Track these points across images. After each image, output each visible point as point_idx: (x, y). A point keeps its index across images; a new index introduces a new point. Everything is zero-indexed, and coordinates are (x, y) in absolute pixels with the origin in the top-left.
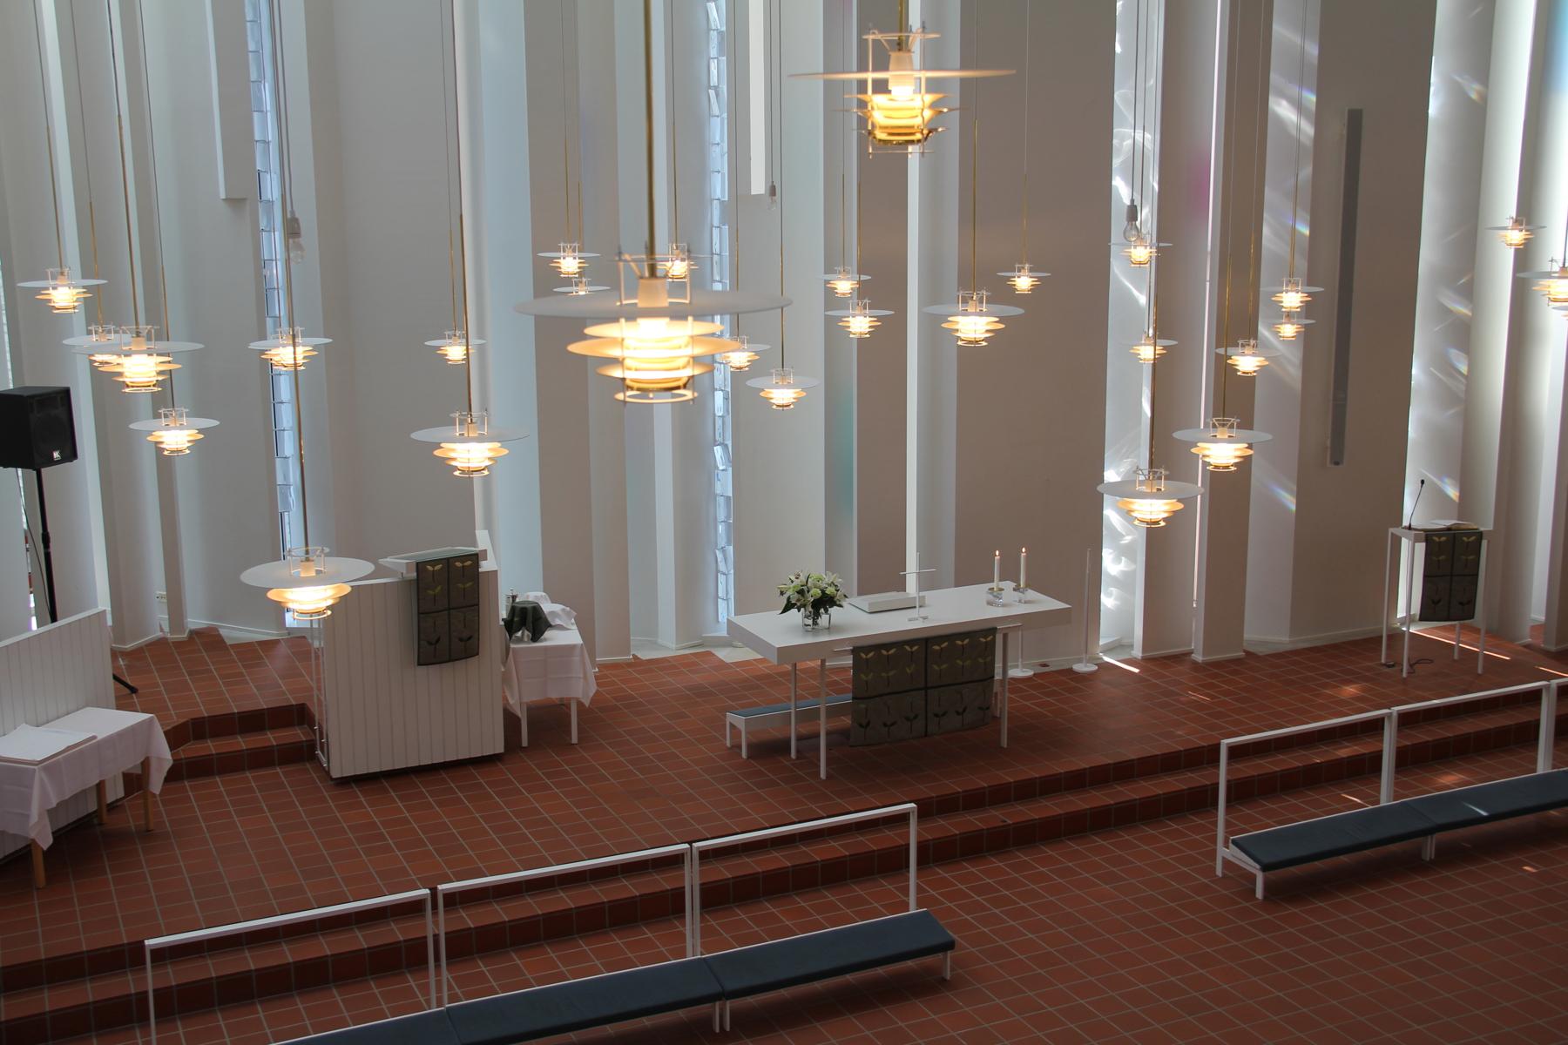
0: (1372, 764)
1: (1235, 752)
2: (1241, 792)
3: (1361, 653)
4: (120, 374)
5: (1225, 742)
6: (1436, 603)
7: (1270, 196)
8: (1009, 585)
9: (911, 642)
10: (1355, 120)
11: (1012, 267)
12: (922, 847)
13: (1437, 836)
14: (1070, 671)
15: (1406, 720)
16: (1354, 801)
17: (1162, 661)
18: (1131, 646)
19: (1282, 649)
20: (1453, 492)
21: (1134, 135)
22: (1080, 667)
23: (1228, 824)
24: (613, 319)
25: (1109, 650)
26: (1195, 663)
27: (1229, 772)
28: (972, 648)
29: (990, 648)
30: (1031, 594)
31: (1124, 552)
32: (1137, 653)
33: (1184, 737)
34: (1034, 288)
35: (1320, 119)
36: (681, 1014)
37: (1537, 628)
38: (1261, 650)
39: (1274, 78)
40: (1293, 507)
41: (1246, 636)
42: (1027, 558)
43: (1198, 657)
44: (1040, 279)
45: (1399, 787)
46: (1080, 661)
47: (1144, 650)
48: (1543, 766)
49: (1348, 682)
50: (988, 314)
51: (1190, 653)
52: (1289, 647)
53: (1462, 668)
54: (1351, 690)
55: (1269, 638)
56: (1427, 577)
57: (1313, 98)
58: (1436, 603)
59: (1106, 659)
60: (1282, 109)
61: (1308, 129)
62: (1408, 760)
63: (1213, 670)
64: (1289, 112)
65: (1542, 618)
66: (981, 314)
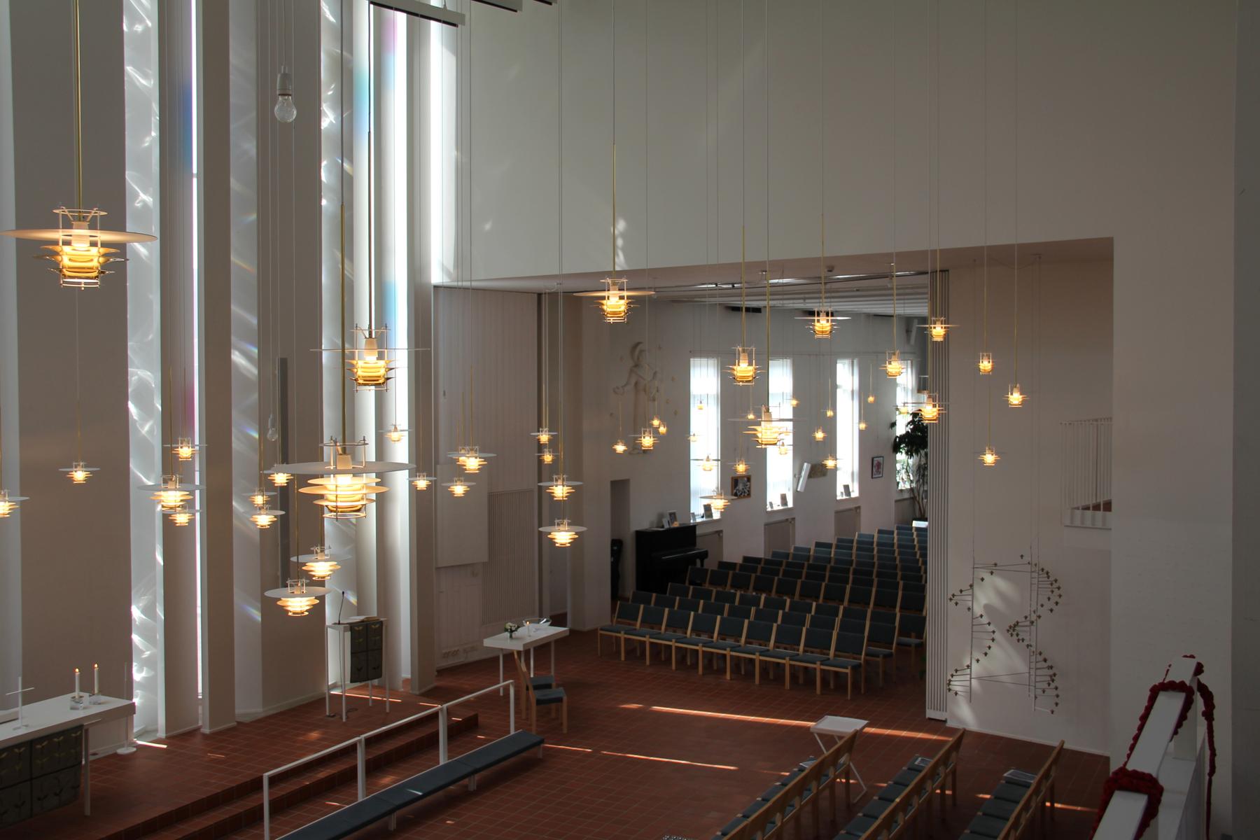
0: (351, 775)
1: (273, 780)
2: (278, 807)
3: (313, 709)
4: (322, 497)
5: (266, 775)
6: (359, 670)
7: (235, 415)
8: (86, 695)
9: (19, 746)
10: (284, 363)
11: (71, 464)
12: (271, 803)
13: (477, 777)
14: (116, 755)
15: (369, 741)
16: (336, 806)
17: (180, 737)
18: (156, 731)
19: (260, 716)
20: (353, 600)
21: (143, 374)
22: (121, 751)
23: (272, 830)
24: (316, 477)
25: (141, 735)
26: (204, 735)
27: (270, 794)
28: (68, 740)
29: (78, 739)
30: (103, 698)
31: (149, 663)
32: (162, 734)
33: (243, 776)
34: (88, 479)
35: (261, 363)
36: (513, 760)
37: (406, 681)
38: (247, 720)
39: (233, 339)
40: (260, 619)
41: (238, 711)
42: (81, 676)
43: (207, 731)
44: (91, 472)
45: (451, 752)
46: (123, 746)
47: (167, 731)
48: (443, 760)
49: (311, 730)
50: (180, 490)
51: (199, 728)
52: (263, 715)
53: (373, 713)
54: (314, 735)
55: (253, 710)
56: (352, 654)
57: (256, 351)
58: (359, 670)
59: (140, 742)
60: (237, 357)
61: (255, 371)
62: (374, 768)
63: (218, 739)
64: (242, 360)
65: (409, 676)
66: (176, 490)
